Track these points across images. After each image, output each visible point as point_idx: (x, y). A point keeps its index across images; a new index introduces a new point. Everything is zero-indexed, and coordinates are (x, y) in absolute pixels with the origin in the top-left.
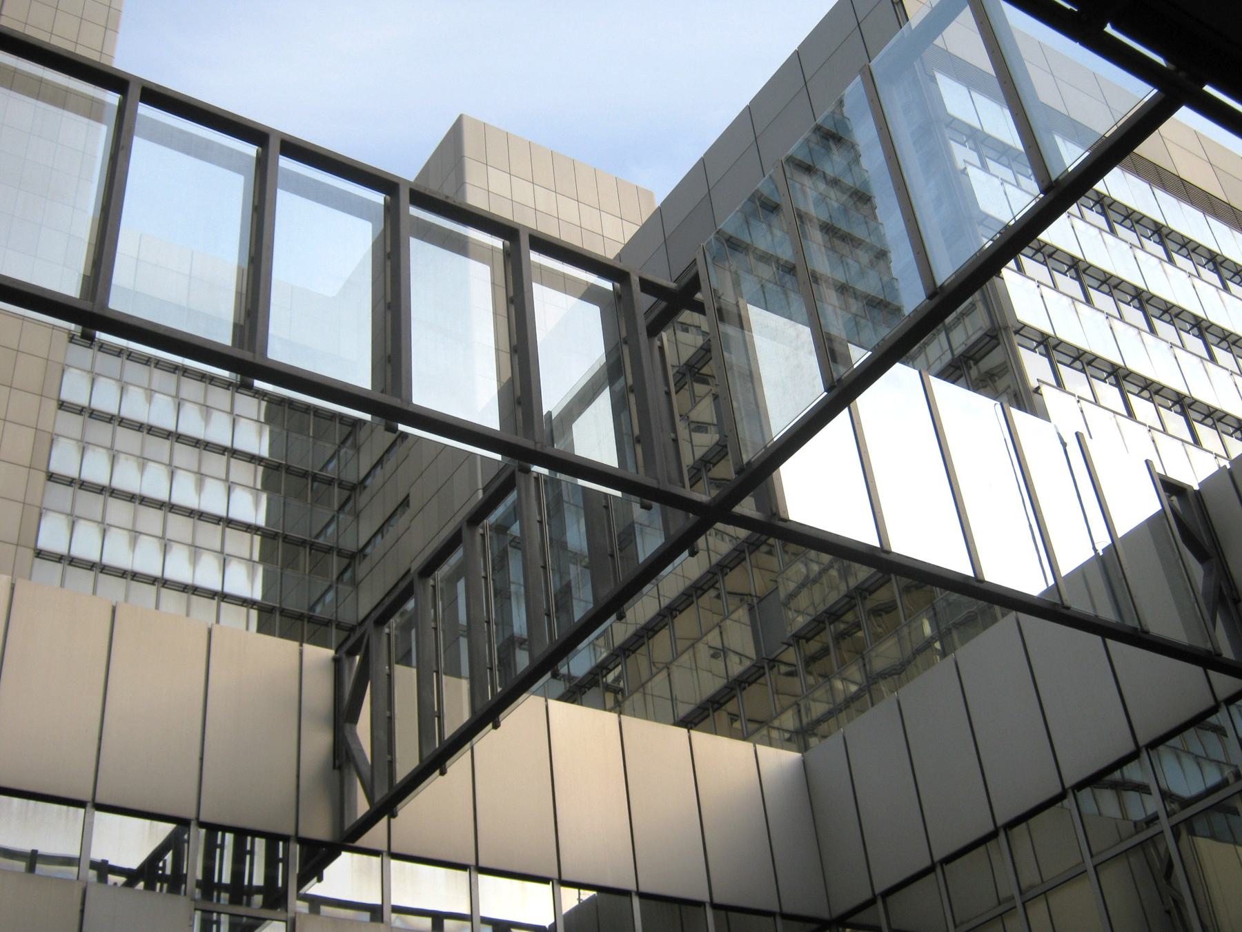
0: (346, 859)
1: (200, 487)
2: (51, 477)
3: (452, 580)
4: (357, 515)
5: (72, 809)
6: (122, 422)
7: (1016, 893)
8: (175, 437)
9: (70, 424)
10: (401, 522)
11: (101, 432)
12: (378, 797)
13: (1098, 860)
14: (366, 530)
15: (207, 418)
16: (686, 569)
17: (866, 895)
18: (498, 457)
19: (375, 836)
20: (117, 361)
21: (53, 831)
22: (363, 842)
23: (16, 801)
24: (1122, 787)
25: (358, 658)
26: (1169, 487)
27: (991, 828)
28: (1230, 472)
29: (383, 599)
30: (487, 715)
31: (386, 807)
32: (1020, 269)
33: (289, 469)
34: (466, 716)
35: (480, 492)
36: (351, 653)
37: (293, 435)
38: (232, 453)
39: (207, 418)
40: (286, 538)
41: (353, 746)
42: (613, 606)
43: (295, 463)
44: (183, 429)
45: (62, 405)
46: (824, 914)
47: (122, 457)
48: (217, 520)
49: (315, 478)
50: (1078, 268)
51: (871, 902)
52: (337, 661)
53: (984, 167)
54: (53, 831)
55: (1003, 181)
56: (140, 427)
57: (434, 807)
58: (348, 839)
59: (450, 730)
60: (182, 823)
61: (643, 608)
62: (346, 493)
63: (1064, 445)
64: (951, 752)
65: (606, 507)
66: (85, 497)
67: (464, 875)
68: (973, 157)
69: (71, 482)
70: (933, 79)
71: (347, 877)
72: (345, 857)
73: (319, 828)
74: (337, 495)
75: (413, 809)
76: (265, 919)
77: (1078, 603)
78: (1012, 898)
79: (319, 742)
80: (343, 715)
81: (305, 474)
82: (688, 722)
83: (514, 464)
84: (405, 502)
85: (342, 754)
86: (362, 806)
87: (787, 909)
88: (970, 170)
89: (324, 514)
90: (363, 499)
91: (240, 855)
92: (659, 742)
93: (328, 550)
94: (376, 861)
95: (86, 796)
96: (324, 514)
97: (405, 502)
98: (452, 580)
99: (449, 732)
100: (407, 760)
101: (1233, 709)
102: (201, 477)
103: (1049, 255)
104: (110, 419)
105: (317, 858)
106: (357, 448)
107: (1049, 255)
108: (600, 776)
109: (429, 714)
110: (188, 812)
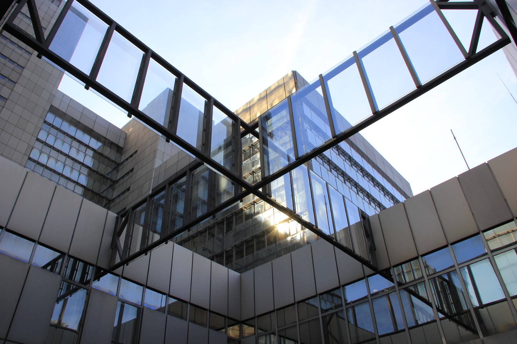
0: (108, 276)
1: (71, 171)
2: (30, 159)
3: (141, 212)
4: (114, 190)
5: (31, 242)
6: (54, 148)
7: (297, 321)
8: (67, 156)
9: (39, 145)
10: (127, 194)
11: (47, 149)
12: (124, 259)
13: (423, 280)
14: (115, 195)
15: (78, 153)
16: (208, 222)
17: (253, 316)
18: (194, 156)
19: (119, 271)
20: (56, 131)
21: (21, 250)
22: (116, 271)
23: (14, 236)
24: (334, 295)
25: (124, 219)
26: (363, 216)
27: (293, 302)
28: (378, 215)
29: (121, 211)
30: (164, 240)
31: (126, 262)
32: (316, 159)
33: (97, 173)
34: (138, 249)
35: (151, 190)
36: (122, 216)
37: (101, 164)
38: (83, 164)
39: (78, 153)
40: (92, 191)
41: (118, 243)
42: (187, 227)
43: (99, 171)
44: (70, 155)
45: (38, 139)
46: (239, 319)
47: (51, 158)
48: (74, 182)
49: (104, 177)
50: (329, 162)
51: (254, 318)
52: (117, 218)
53: (311, 131)
54: (21, 250)
55: (315, 135)
56: (58, 151)
57: (137, 266)
58: (111, 270)
59: (132, 253)
60: (63, 254)
61: (194, 230)
62: (112, 183)
63: (326, 204)
64: (269, 286)
65: (191, 200)
66: (38, 167)
67: (142, 287)
68: (309, 127)
69: (35, 161)
70: (302, 104)
71: (107, 283)
72: (109, 274)
73: (103, 264)
74: (109, 183)
75: (133, 264)
76: (81, 287)
77: (341, 239)
78: (296, 322)
79: (108, 239)
80: (117, 234)
81: (102, 175)
82: (212, 259)
83: (199, 160)
84: (128, 189)
85: (114, 245)
86: (118, 260)
87: (229, 316)
88: (308, 130)
89: (104, 187)
90: (117, 185)
91: (74, 269)
92: (203, 263)
93: (104, 197)
94: (118, 278)
95: (36, 239)
96: (104, 187)
97: (128, 189)
98: (141, 212)
99: (131, 254)
100: (137, 247)
101: (395, 268)
102: (72, 169)
103: (324, 158)
104: (50, 146)
105: (99, 274)
106: (118, 172)
107: (324, 158)
108: (183, 268)
109: (145, 237)
110: (66, 251)
